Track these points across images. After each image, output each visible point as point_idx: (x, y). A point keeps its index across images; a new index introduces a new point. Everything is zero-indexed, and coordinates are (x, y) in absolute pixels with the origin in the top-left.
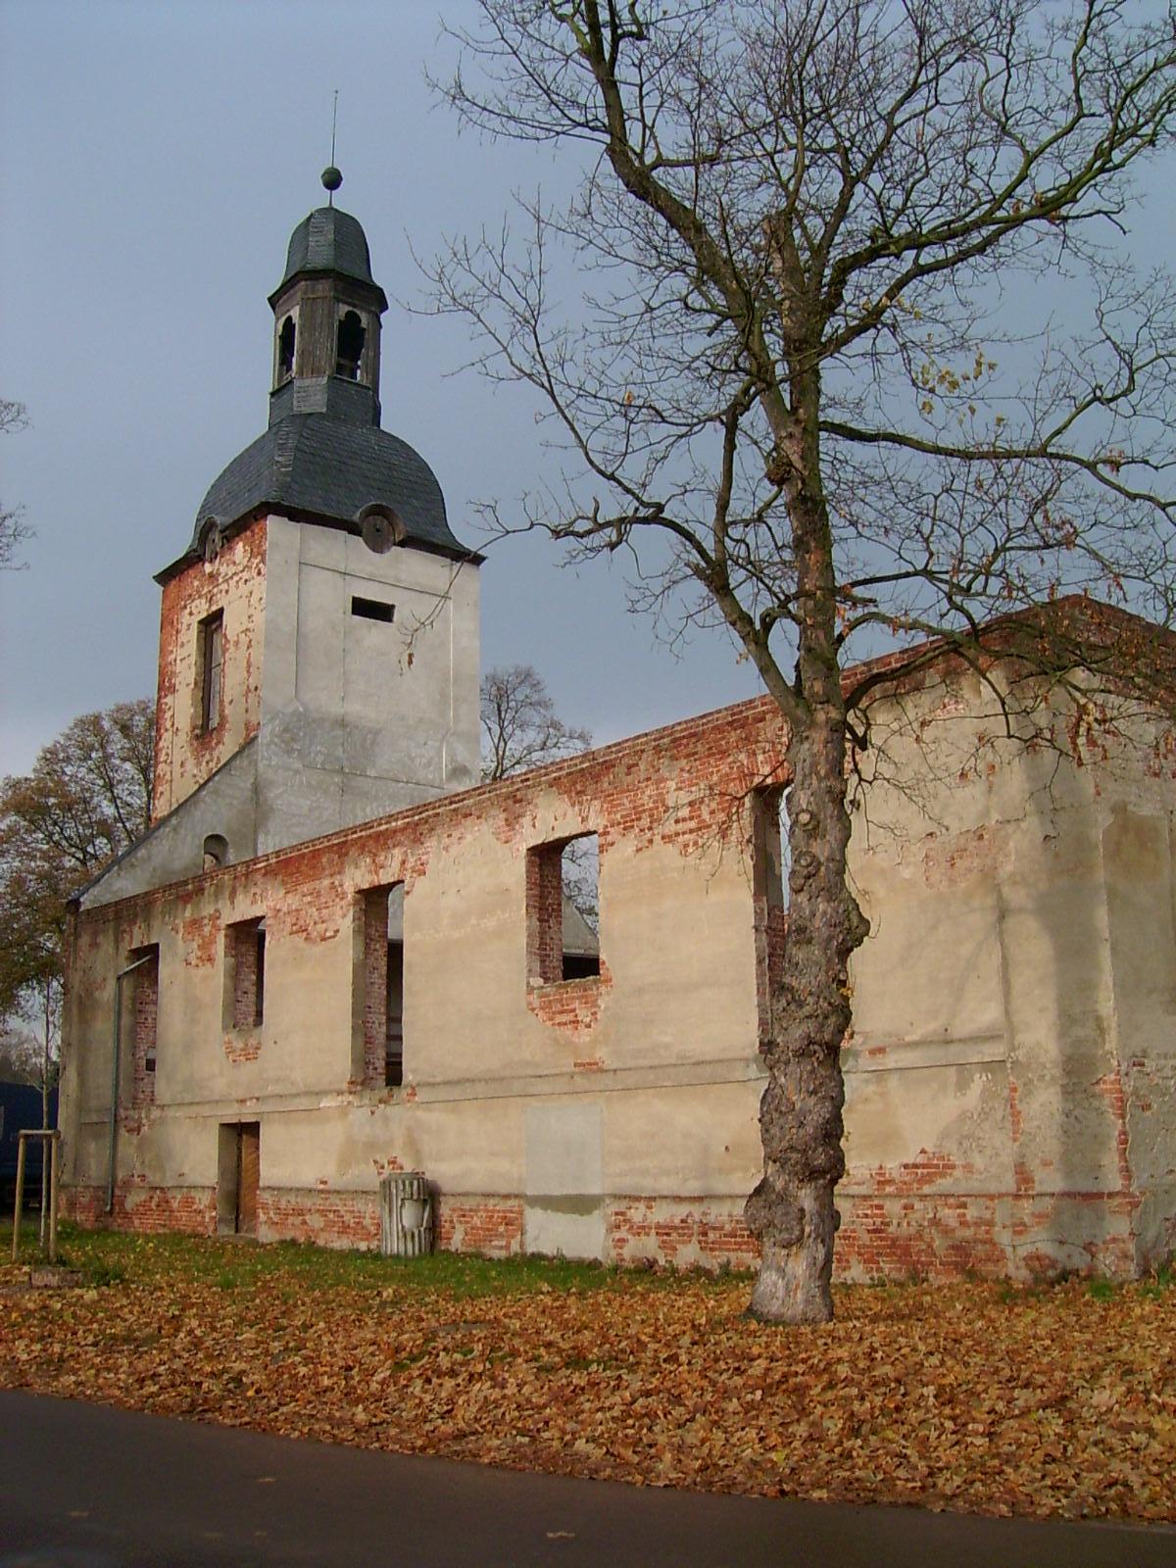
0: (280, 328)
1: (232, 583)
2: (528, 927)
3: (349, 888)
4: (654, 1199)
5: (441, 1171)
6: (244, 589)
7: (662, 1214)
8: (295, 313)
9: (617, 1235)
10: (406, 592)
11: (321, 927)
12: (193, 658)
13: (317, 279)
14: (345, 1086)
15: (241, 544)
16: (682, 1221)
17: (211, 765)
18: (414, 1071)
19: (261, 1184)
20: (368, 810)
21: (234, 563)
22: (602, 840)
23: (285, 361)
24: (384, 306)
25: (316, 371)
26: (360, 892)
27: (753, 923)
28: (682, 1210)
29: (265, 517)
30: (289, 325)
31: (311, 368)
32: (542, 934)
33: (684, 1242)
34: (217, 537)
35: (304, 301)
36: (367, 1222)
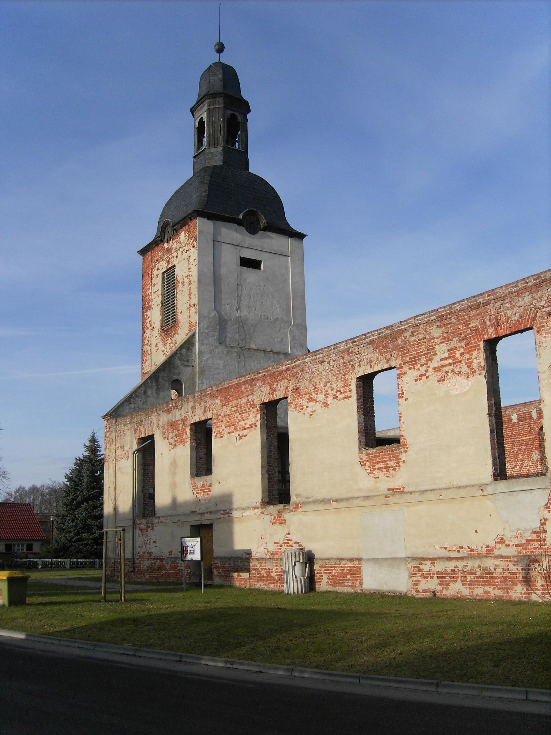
0: (197, 124)
1: (179, 253)
2: (359, 419)
3: (258, 403)
4: (435, 559)
5: (319, 549)
6: (186, 255)
7: (439, 567)
8: (205, 116)
9: (415, 579)
10: (267, 254)
11: (242, 423)
12: (160, 292)
13: (215, 98)
14: (259, 504)
15: (183, 233)
16: (452, 570)
17: (172, 345)
18: (297, 496)
19: (214, 556)
20: (253, 365)
21: (180, 242)
22: (399, 372)
23: (200, 142)
24: (249, 111)
25: (216, 145)
26: (263, 404)
27: (487, 412)
28: (451, 565)
29: (195, 218)
30: (201, 122)
31: (213, 143)
32: (366, 422)
33: (453, 581)
34: (170, 229)
35: (209, 110)
36: (273, 574)
